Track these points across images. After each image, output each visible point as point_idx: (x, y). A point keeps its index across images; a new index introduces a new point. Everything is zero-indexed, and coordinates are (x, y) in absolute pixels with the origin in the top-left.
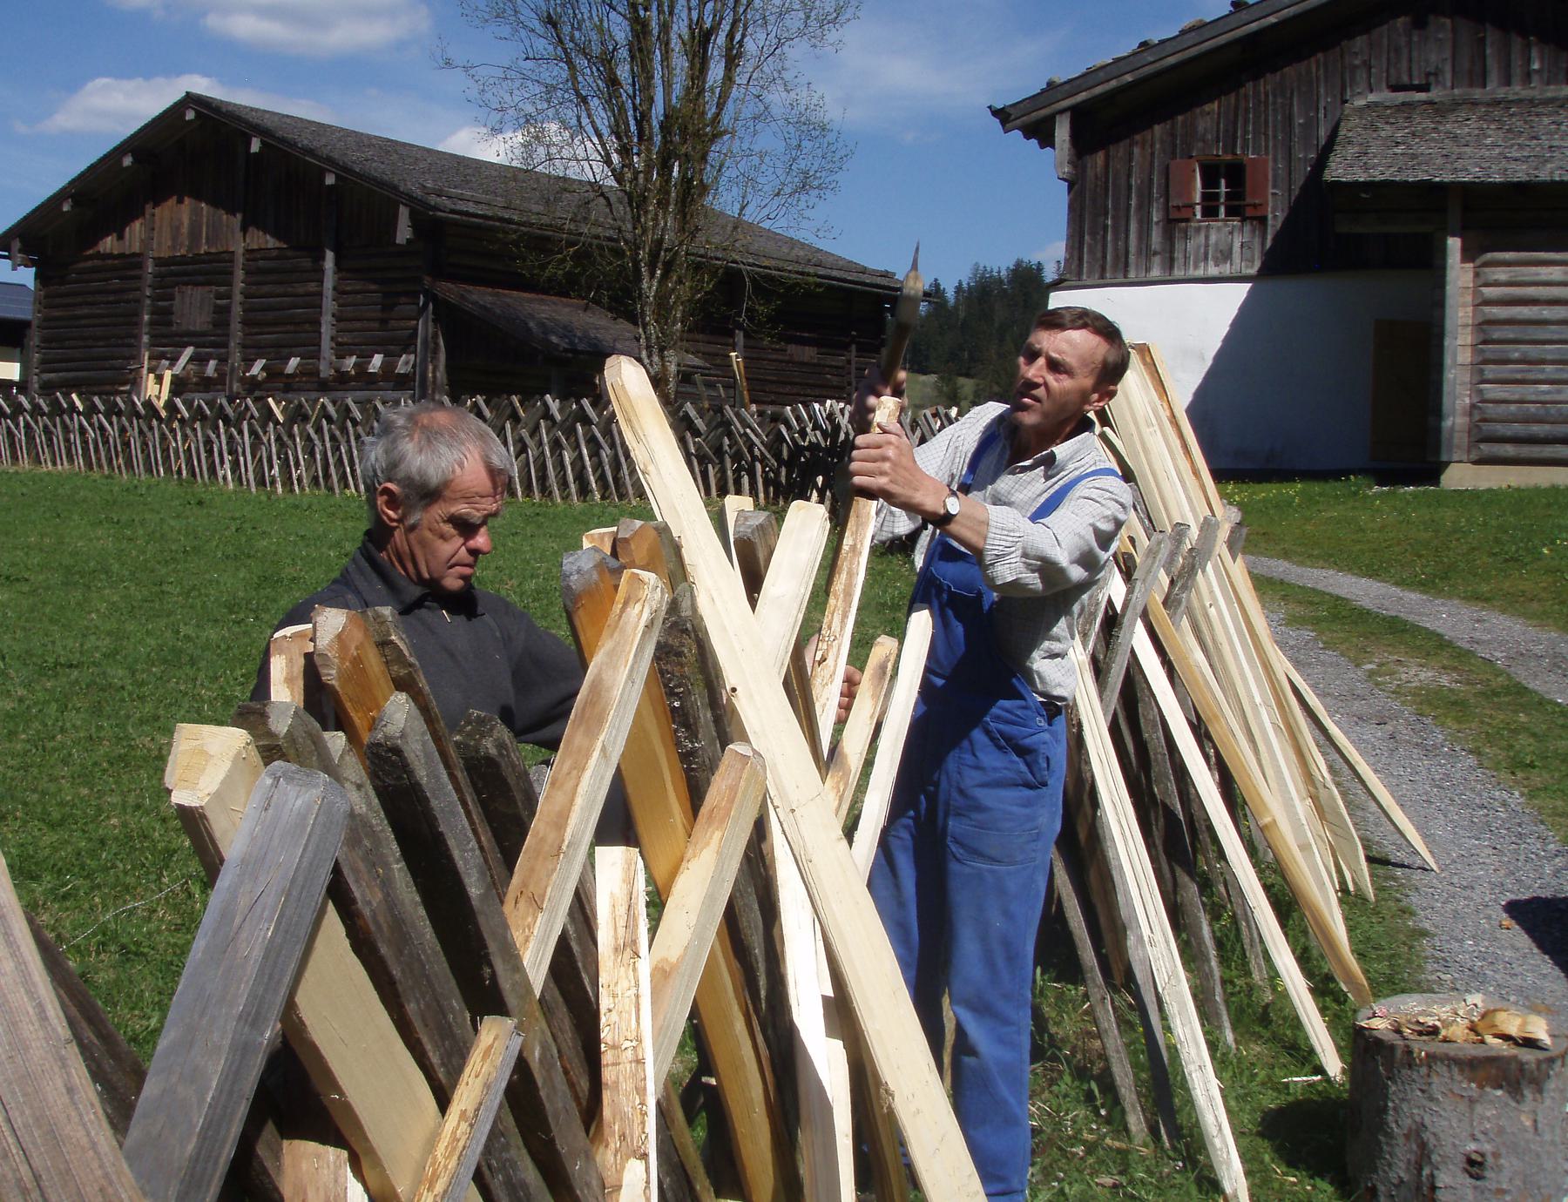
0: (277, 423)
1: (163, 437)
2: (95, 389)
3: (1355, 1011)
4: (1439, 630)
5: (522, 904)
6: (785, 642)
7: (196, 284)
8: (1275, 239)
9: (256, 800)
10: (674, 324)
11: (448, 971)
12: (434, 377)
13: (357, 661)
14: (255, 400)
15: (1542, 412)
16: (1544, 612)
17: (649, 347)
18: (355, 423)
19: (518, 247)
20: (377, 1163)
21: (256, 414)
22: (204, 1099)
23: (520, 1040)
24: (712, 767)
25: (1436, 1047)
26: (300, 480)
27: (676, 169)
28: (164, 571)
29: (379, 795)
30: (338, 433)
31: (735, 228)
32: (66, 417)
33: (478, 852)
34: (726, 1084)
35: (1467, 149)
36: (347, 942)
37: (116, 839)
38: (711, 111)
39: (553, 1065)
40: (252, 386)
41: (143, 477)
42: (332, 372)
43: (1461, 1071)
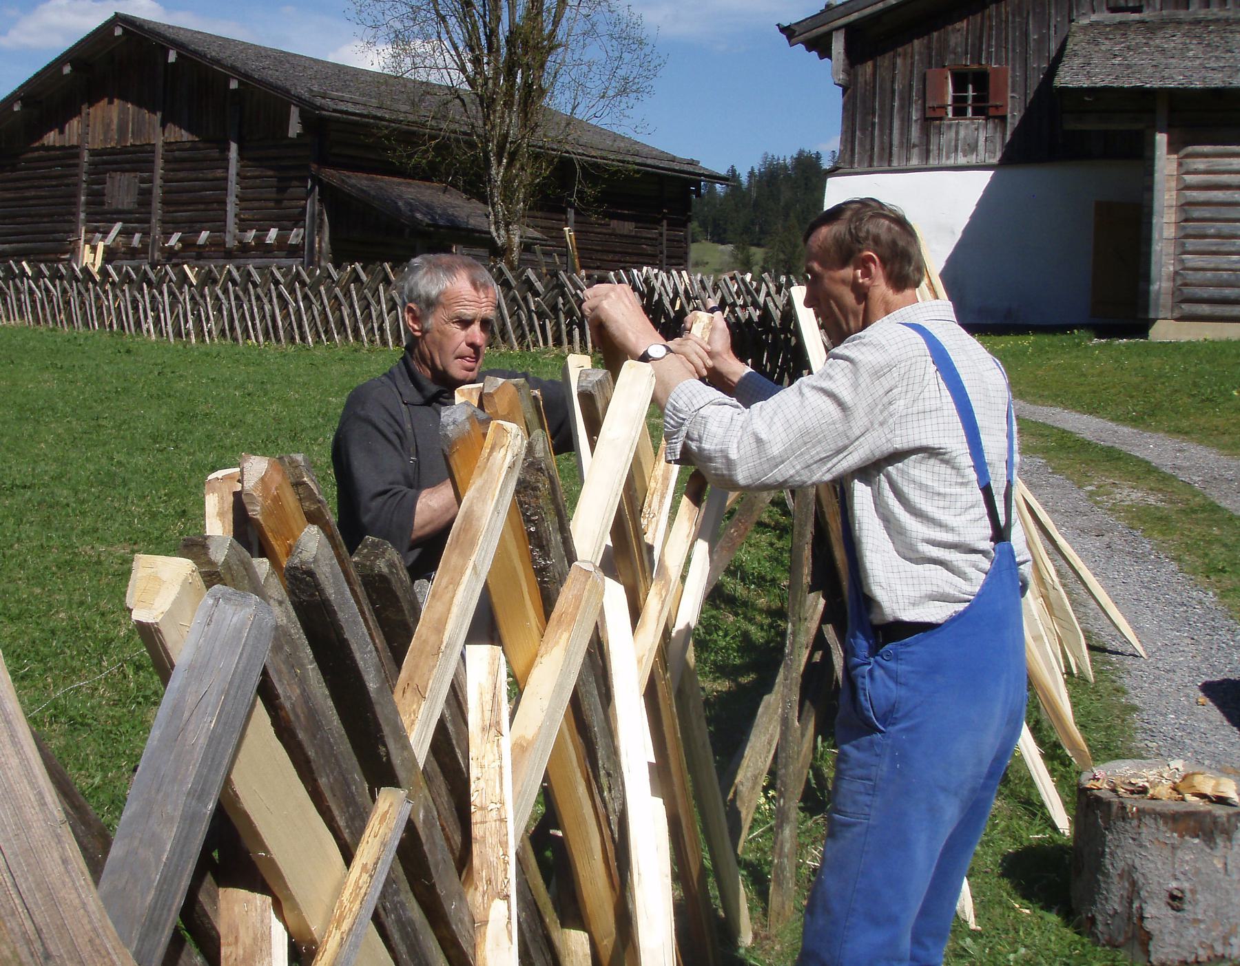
0: (191, 285)
1: (98, 297)
2: (42, 257)
3: (1079, 773)
4: (1147, 458)
5: (408, 694)
6: (619, 476)
7: (124, 171)
8: (1013, 134)
9: (200, 617)
10: (518, 203)
11: (351, 750)
12: (320, 247)
13: (277, 499)
14: (174, 266)
15: (1233, 278)
16: (1234, 444)
17: (496, 223)
18: (255, 285)
19: (389, 140)
20: (295, 907)
21: (174, 278)
22: (160, 860)
23: (409, 807)
24: (561, 580)
25: (1145, 804)
26: (210, 332)
27: (519, 75)
28: (100, 408)
29: (296, 608)
30: (241, 293)
31: (568, 124)
32: (18, 281)
33: (374, 653)
34: (570, 836)
35: (1172, 60)
36: (272, 730)
37: (64, 630)
38: (548, 28)
39: (434, 825)
40: (170, 254)
41: (81, 330)
42: (236, 243)
43: (1166, 823)
